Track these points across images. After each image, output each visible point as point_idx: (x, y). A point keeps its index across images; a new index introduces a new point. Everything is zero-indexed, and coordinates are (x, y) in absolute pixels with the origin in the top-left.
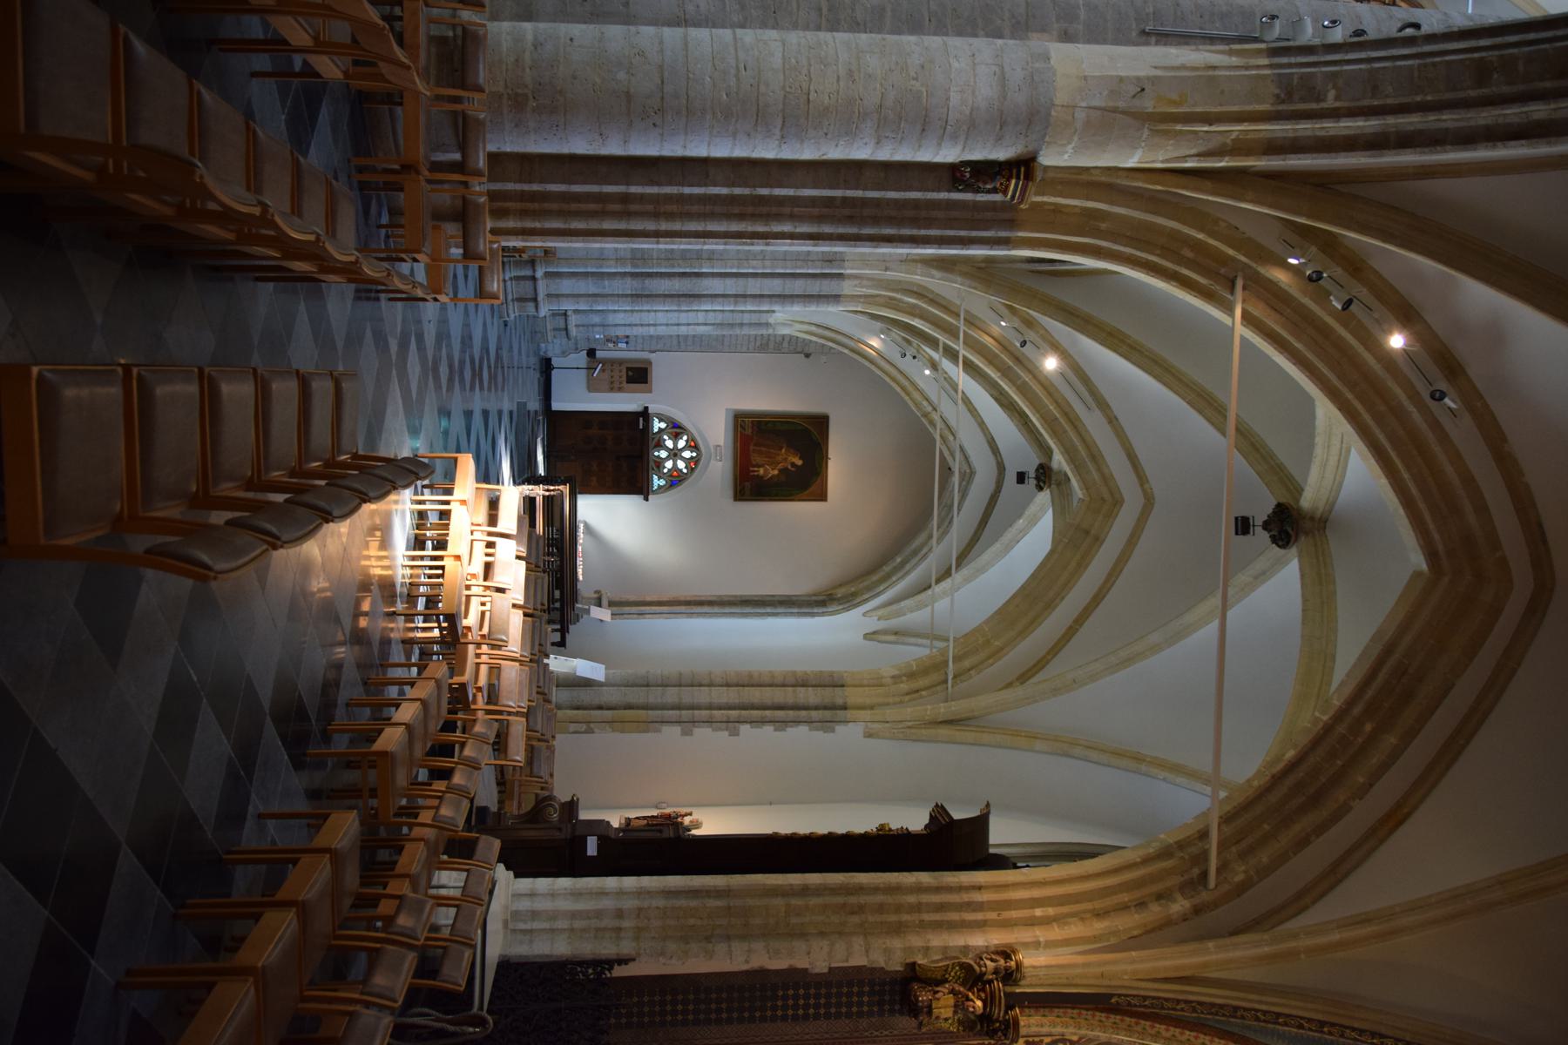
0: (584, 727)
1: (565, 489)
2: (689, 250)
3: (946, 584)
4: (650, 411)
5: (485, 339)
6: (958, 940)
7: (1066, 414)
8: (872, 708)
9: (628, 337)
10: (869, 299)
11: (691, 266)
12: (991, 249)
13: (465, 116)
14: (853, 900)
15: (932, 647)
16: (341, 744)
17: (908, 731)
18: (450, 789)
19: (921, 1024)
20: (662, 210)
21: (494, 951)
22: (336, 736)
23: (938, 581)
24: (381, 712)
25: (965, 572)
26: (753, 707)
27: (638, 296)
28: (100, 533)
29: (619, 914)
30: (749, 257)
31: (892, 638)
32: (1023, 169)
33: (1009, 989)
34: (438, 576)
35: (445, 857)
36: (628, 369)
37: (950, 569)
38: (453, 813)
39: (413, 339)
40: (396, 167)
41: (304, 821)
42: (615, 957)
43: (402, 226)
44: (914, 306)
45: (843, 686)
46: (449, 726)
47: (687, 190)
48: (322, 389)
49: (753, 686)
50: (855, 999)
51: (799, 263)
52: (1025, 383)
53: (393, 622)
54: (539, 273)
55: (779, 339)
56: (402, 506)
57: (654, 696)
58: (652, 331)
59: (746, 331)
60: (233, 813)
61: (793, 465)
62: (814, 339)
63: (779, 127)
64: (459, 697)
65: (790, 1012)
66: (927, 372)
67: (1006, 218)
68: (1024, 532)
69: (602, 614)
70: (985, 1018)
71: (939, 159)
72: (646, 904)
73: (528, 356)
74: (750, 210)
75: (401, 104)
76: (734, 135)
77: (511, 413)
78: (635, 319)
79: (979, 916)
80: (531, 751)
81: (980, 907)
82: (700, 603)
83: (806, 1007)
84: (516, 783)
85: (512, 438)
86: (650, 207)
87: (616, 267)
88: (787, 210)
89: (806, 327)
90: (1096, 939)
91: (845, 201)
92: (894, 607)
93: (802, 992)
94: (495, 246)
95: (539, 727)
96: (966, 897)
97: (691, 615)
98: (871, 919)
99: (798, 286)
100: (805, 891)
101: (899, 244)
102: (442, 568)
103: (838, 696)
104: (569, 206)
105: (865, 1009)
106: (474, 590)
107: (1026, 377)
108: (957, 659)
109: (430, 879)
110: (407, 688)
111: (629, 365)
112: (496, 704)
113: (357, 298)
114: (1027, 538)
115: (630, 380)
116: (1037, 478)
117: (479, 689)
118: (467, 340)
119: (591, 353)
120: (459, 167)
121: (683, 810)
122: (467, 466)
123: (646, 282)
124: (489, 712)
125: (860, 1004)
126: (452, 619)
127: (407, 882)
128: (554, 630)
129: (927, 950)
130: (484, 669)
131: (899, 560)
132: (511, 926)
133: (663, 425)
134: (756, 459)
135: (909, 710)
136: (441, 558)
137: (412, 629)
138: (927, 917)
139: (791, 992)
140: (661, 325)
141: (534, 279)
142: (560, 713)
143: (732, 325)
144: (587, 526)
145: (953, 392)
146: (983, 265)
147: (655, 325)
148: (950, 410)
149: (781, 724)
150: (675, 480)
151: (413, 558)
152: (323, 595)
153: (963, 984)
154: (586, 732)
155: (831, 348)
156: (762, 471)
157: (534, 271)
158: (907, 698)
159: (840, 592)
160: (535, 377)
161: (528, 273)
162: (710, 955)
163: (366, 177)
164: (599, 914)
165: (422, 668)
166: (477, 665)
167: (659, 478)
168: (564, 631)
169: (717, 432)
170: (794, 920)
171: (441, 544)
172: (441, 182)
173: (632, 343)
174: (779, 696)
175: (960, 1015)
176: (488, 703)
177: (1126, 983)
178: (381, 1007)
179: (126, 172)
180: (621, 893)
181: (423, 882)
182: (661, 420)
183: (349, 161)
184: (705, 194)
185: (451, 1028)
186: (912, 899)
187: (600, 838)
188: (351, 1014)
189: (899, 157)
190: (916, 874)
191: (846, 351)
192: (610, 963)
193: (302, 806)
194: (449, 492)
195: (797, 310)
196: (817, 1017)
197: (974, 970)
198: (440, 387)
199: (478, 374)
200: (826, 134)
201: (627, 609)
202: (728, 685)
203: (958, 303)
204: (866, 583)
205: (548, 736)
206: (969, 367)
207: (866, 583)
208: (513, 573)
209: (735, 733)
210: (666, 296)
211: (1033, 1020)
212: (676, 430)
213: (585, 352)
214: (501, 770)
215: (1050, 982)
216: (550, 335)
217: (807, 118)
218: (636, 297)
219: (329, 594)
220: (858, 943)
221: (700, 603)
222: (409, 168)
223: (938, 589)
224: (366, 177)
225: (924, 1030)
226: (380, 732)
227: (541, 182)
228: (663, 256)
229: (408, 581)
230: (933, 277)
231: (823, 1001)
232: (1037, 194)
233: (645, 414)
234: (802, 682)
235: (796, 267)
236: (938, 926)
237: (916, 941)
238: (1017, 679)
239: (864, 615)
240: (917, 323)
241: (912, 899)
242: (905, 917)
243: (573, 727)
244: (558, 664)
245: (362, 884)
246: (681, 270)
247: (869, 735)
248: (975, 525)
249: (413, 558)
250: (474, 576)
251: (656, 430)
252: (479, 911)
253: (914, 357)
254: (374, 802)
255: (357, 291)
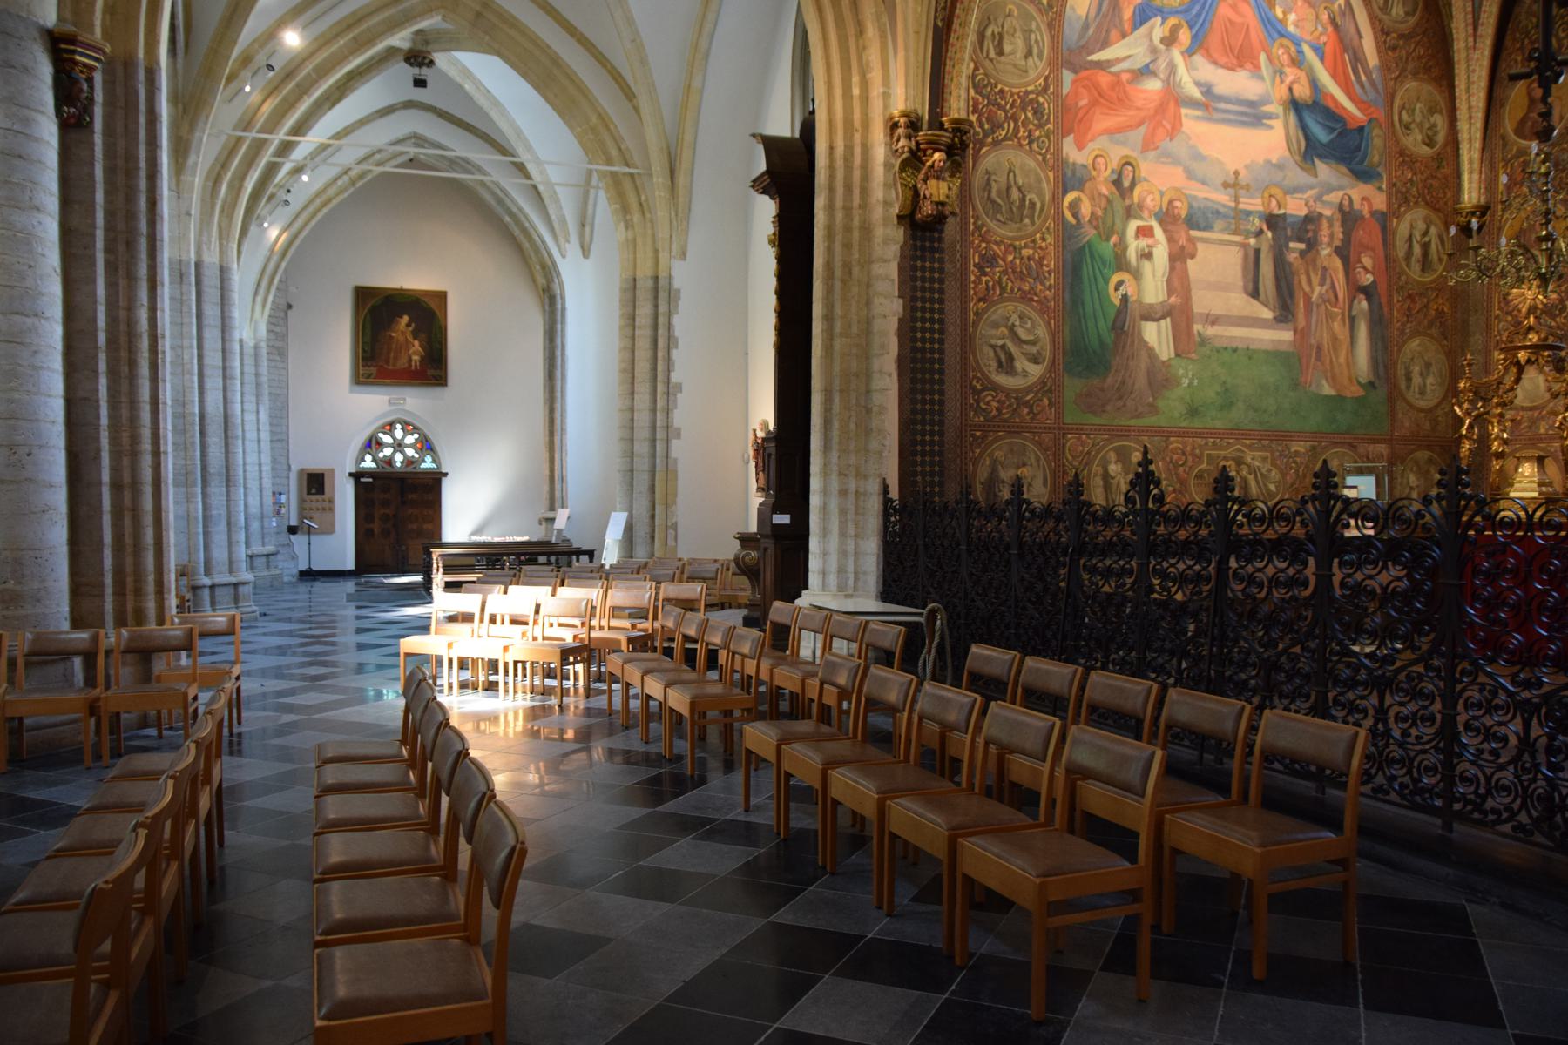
0: (671, 532)
1: (436, 553)
2: (174, 427)
3: (530, 167)
4: (353, 471)
5: (280, 634)
6: (879, 173)
7: (349, 27)
8: (656, 252)
9: (274, 493)
10: (223, 236)
11: (193, 424)
12: (160, 90)
13: (31, 654)
14: (838, 273)
15: (597, 188)
16: (683, 746)
17: (680, 215)
18: (726, 645)
19: (953, 214)
20: (128, 448)
21: (873, 605)
22: (676, 751)
23: (529, 177)
24: (653, 713)
25: (520, 150)
26: (654, 369)
27: (228, 480)
28: (482, 959)
29: (843, 493)
30: (179, 362)
31: (588, 229)
32: (63, 46)
33: (925, 126)
34: (524, 668)
35: (788, 652)
36: (309, 493)
37: (514, 164)
38: (748, 640)
39: (281, 700)
40: (93, 721)
41: (752, 772)
42: (881, 497)
43: (159, 712)
44: (230, 186)
45: (635, 280)
46: (668, 652)
47: (104, 421)
48: (332, 775)
49: (633, 369)
50: (927, 274)
51: (185, 309)
52: (316, 69)
53: (568, 707)
54: (207, 581)
55: (272, 336)
56: (458, 704)
57: (642, 465)
58: (266, 468)
59: (264, 370)
60: (745, 833)
61: (408, 325)
62: (270, 298)
63: (24, 319)
64: (640, 644)
65: (936, 336)
66: (305, 178)
67: (122, 70)
68: (478, 84)
69: (562, 518)
70: (950, 151)
71: (54, 141)
72: (835, 468)
73: (297, 593)
74: (124, 354)
75: (21, 719)
76: (36, 368)
77: (359, 607)
78: (253, 485)
79: (858, 150)
80: (692, 579)
81: (849, 149)
82: (552, 421)
83: (932, 321)
84: (723, 593)
85: (384, 606)
86: (126, 461)
87: (197, 502)
88: (122, 314)
89: (258, 307)
90: (883, 36)
91: (108, 250)
92: (556, 226)
93: (919, 325)
94: (176, 620)
95: (671, 572)
96: (840, 163)
97: (563, 430)
98: (856, 256)
99: (212, 311)
100: (828, 318)
101: (158, 192)
102: (516, 663)
103: (645, 284)
104: (131, 547)
105: (936, 265)
106: (538, 633)
107: (309, 67)
108: (609, 162)
109: (807, 663)
110: (632, 692)
111: (305, 491)
112: (648, 610)
113: (240, 753)
114: (485, 82)
115: (321, 491)
116: (420, 65)
117: (633, 626)
118: (281, 650)
119: (292, 530)
120: (89, 657)
121: (751, 437)
122: (413, 643)
123: (212, 471)
124: (655, 618)
125: (932, 270)
126: (566, 654)
127: (808, 681)
128: (578, 560)
129: (887, 204)
130: (615, 623)
131: (507, 219)
132: (850, 592)
133: (368, 458)
134: (402, 363)
135: (659, 213)
136: (506, 664)
137: (576, 690)
138: (856, 200)
139: (919, 335)
140: (260, 459)
141: (212, 587)
142: (657, 554)
143: (258, 385)
144: (474, 533)
145: (330, 149)
146: (180, 106)
147: (260, 465)
148: (349, 155)
149: (671, 341)
150: (426, 445)
151: (506, 691)
152: (542, 769)
153: (919, 170)
154: (676, 530)
155: (281, 281)
156: (416, 358)
157: (204, 586)
158: (648, 215)
159: (541, 281)
160: (319, 587)
161: (206, 593)
162: (883, 409)
163: (106, 752)
164: (843, 512)
165: (613, 678)
166: (614, 630)
167: (424, 461)
168: (579, 553)
169: (375, 403)
170: (855, 329)
171: (493, 666)
172: (107, 676)
173: (280, 489)
174: (643, 344)
175: (947, 175)
176: (647, 619)
177: (925, 9)
178: (917, 690)
179: (107, 963)
180: (825, 492)
181: (809, 668)
182: (363, 460)
183: (89, 768)
184: (108, 402)
185: (936, 640)
186: (839, 216)
187: (774, 511)
188: (920, 719)
189: (54, 186)
190: (816, 211)
191: (284, 265)
192: (887, 501)
193: (738, 777)
194: (439, 660)
195: (238, 313)
196: (941, 311)
197: (906, 159)
198: (332, 673)
199: (317, 640)
200: (30, 267)
201: (558, 494)
202: (633, 393)
203: (224, 138)
204: (532, 255)
205: (680, 564)
206: (300, 129)
207: (532, 255)
208: (521, 597)
209: (679, 387)
210: (227, 452)
211: (954, 105)
212: (372, 444)
213: (292, 537)
214: (710, 607)
215: (920, 85)
216: (274, 572)
217: (12, 287)
218: (229, 481)
219: (541, 764)
220: (878, 269)
221: (552, 421)
222: (93, 708)
223: (537, 178)
224: (106, 752)
225: (957, 211)
226: (672, 710)
227: (102, 575)
228: (183, 453)
229: (529, 695)
230: (196, 164)
231: (928, 305)
232: (93, 33)
233: (357, 476)
234: (631, 319)
235: (190, 311)
236: (865, 192)
237: (878, 214)
238: (631, 101)
239: (564, 257)
240: (250, 184)
241: (839, 216)
242: (856, 222)
243: (671, 543)
244: (610, 555)
245: (810, 717)
246: (198, 435)
247: (683, 255)
248: (471, 137)
249: (506, 691)
250: (524, 634)
251: (374, 465)
252: (836, 617)
253: (289, 191)
254: (737, 713)
255: (231, 753)
